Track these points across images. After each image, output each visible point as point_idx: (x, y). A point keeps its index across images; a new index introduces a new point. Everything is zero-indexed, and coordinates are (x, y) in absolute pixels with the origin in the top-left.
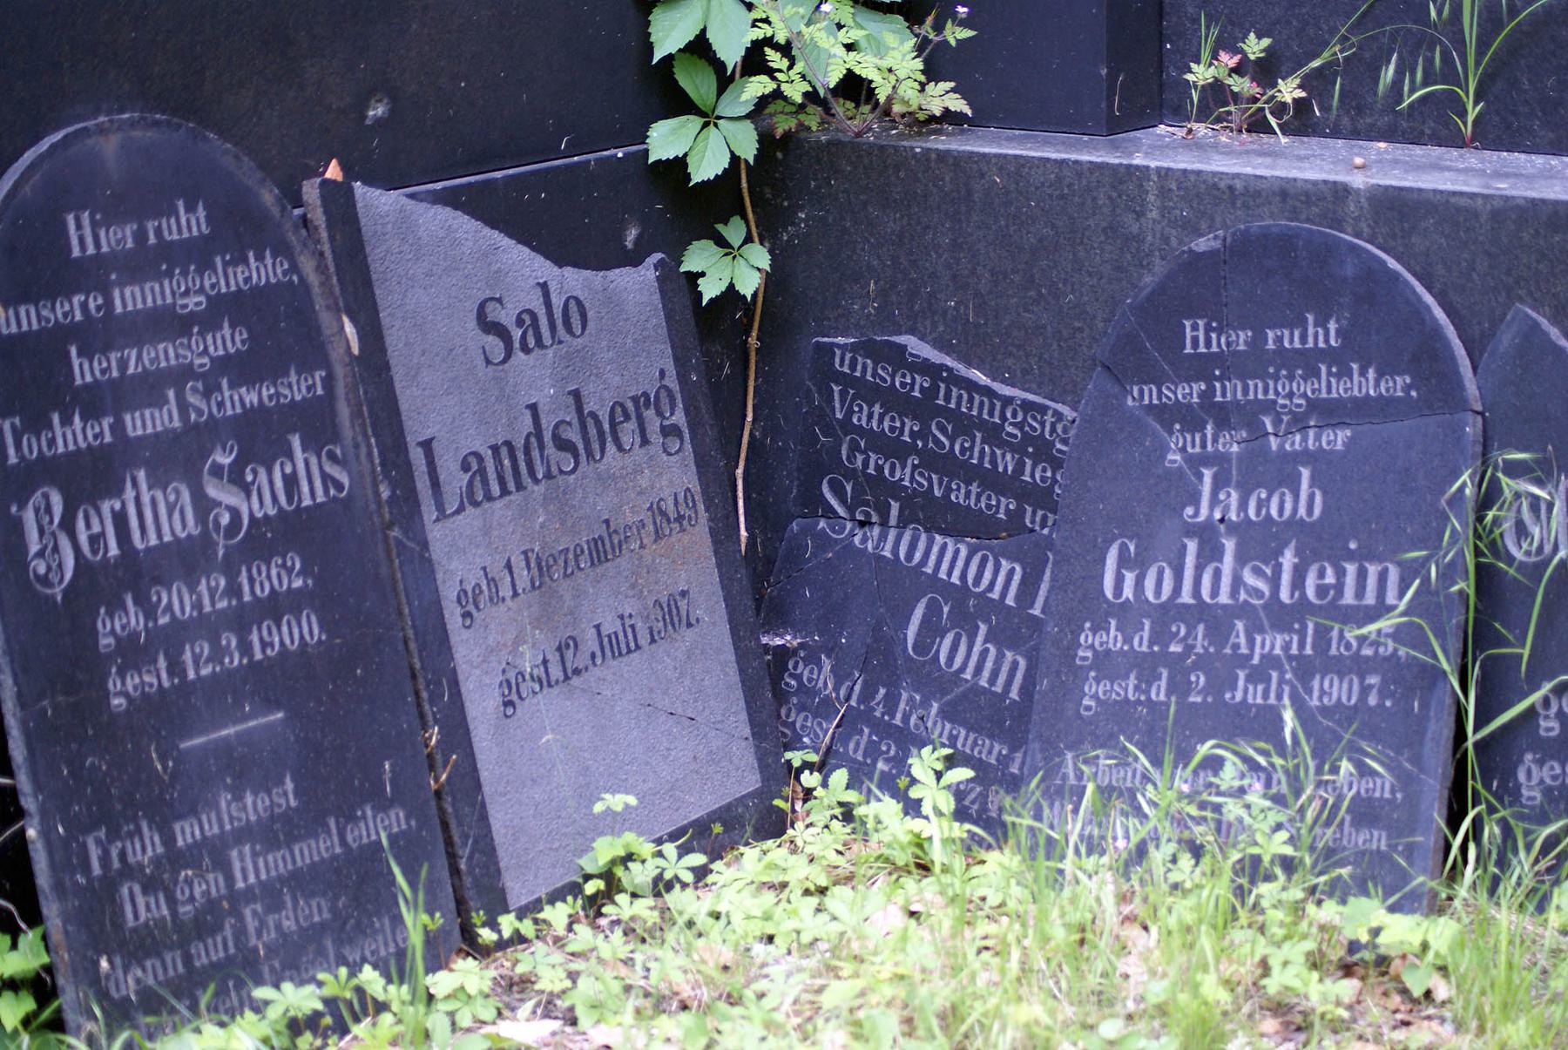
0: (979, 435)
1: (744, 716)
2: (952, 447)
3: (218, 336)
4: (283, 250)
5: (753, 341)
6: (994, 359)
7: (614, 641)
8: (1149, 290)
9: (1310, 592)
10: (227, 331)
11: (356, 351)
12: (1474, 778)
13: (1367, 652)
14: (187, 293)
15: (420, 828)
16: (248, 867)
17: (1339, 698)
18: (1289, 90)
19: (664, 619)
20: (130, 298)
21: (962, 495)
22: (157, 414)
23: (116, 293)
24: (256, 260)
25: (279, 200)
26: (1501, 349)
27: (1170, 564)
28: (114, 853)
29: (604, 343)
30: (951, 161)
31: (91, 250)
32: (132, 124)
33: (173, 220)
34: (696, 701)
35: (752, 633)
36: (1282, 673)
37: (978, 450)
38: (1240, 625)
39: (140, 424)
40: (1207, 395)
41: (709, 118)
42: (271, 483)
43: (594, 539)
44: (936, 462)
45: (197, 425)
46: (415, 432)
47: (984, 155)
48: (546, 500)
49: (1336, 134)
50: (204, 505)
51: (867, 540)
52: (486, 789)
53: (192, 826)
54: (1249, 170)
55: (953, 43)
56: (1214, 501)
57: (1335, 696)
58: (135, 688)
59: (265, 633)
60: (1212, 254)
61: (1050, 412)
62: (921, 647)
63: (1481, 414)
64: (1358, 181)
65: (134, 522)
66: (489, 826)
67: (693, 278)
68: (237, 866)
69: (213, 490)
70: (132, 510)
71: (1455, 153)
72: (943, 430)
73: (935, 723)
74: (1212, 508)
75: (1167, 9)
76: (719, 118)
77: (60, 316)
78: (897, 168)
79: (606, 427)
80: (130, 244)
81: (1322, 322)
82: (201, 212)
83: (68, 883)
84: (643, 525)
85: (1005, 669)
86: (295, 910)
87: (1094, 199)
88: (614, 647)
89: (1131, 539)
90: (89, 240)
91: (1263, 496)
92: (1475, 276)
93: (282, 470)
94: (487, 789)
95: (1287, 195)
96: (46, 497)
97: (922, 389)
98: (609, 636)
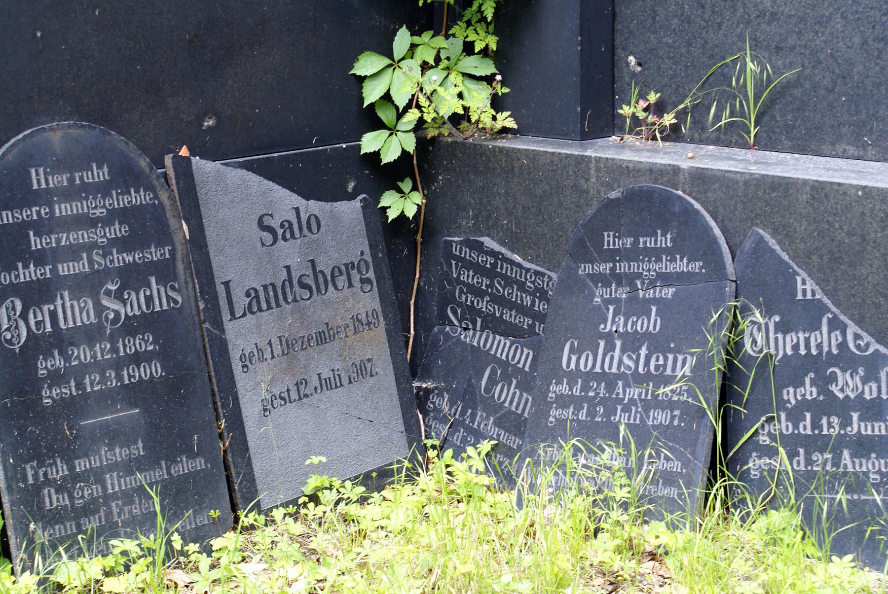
0: (515, 287)
1: (401, 421)
2: (504, 292)
3: (112, 228)
4: (150, 188)
5: (419, 238)
6: (524, 250)
7: (328, 382)
8: (589, 217)
9: (652, 368)
10: (117, 226)
11: (188, 237)
12: (721, 464)
13: (675, 398)
14: (96, 207)
15: (212, 468)
16: (114, 483)
17: (661, 421)
18: (669, 119)
19: (357, 372)
20: (63, 209)
21: (510, 316)
22: (76, 265)
23: (57, 207)
24: (135, 193)
25: (149, 164)
26: (746, 249)
27: (592, 352)
28: (41, 473)
29: (330, 238)
30: (505, 152)
31: (44, 186)
32: (69, 127)
33: (89, 173)
34: (374, 412)
35: (408, 381)
36: (637, 407)
37: (515, 295)
38: (620, 383)
39: (64, 269)
40: (613, 269)
41: (393, 131)
42: (138, 299)
43: (319, 332)
44: (497, 300)
45: (98, 271)
46: (220, 277)
47: (519, 149)
48: (292, 313)
49: (692, 141)
50: (100, 309)
51: (467, 337)
52: (252, 451)
53: (85, 462)
54: (637, 159)
55: (500, 94)
56: (613, 322)
57: (659, 421)
58: (57, 395)
59: (131, 371)
60: (618, 199)
61: (546, 276)
62: (488, 390)
63: (735, 281)
64: (685, 165)
65: (61, 315)
66: (252, 469)
67: (385, 209)
68: (109, 482)
69: (105, 302)
70: (60, 310)
71: (744, 151)
72: (500, 284)
73: (491, 428)
74: (612, 326)
75: (617, 79)
76: (398, 131)
77: (25, 217)
78: (481, 156)
79: (329, 278)
80: (65, 183)
81: (664, 235)
82: (106, 169)
83: (14, 487)
84: (348, 327)
85: (523, 402)
86: (140, 504)
87: (567, 172)
88: (326, 384)
89: (576, 339)
90: (43, 181)
91: (635, 320)
92: (737, 212)
93: (145, 294)
94: (252, 451)
95: (654, 172)
96: (12, 302)
97: (491, 264)
98: (325, 379)
